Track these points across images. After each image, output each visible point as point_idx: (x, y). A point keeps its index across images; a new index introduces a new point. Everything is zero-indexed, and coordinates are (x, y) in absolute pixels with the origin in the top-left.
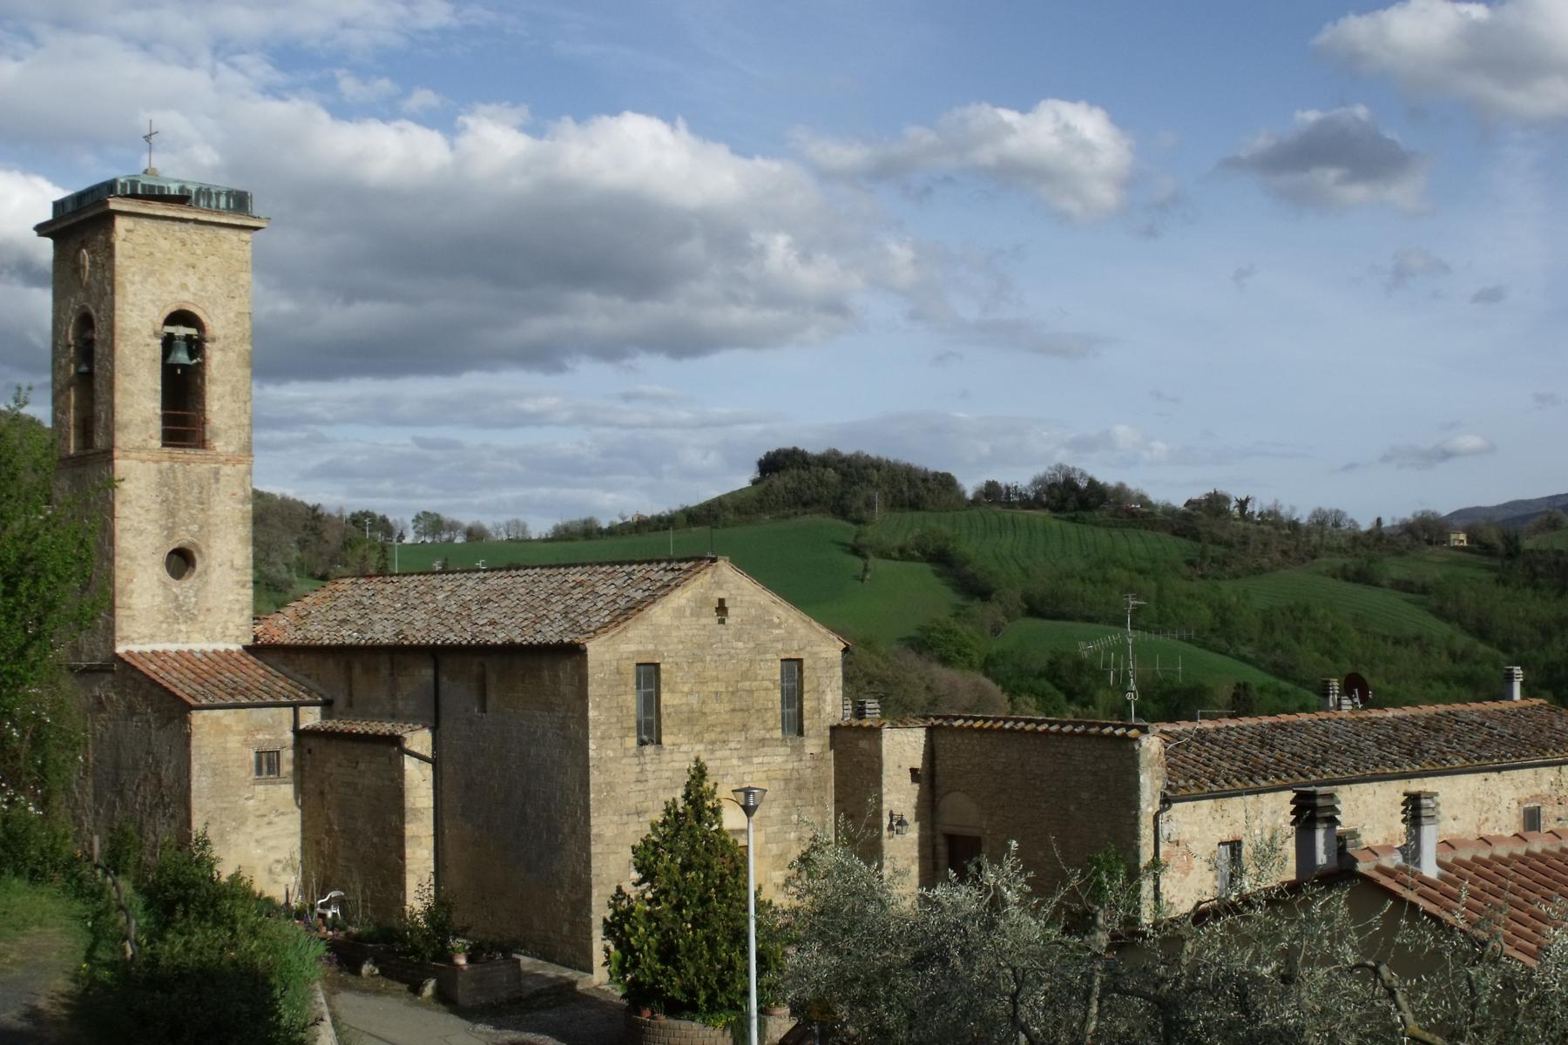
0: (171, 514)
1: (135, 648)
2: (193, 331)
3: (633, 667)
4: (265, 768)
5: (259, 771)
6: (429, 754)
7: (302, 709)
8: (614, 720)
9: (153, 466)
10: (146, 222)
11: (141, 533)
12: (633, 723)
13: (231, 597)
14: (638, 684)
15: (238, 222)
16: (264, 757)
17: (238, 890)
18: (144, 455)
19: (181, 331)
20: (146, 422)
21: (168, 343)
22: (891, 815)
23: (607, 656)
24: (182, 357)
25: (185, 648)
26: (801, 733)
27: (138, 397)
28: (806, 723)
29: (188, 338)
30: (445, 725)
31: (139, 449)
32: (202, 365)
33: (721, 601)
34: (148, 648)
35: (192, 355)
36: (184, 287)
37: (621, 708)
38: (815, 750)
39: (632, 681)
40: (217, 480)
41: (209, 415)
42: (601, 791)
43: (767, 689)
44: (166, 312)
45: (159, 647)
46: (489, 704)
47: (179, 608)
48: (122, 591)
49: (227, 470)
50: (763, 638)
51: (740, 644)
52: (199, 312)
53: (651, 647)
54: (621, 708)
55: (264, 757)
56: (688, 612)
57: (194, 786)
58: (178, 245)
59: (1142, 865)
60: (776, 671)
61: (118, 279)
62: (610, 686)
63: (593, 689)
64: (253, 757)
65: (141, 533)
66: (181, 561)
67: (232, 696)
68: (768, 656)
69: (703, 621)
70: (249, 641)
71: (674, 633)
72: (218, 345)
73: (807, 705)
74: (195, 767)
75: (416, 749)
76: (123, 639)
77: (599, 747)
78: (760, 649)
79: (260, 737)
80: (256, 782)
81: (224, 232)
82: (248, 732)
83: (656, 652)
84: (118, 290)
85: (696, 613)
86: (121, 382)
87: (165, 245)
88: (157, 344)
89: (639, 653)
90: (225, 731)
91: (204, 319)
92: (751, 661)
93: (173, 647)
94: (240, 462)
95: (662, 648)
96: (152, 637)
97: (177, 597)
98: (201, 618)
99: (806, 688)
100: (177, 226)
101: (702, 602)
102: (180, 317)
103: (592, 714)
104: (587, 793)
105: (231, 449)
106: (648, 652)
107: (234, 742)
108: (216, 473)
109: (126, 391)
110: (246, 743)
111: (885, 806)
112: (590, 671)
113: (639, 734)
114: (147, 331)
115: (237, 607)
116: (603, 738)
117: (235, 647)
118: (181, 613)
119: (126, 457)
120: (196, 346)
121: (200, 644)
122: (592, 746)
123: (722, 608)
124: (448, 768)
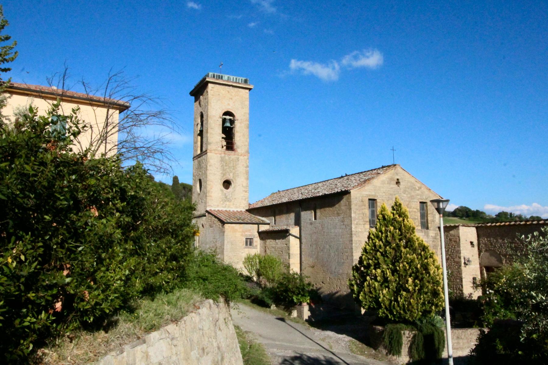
0: (224, 170)
1: (213, 209)
2: (231, 118)
3: (367, 200)
4: (249, 243)
5: (246, 244)
6: (292, 215)
7: (260, 225)
8: (361, 218)
9: (220, 155)
10: (218, 86)
11: (215, 175)
12: (368, 220)
13: (242, 195)
14: (369, 208)
15: (245, 86)
16: (249, 240)
17: (228, 269)
18: (216, 152)
19: (228, 117)
20: (217, 143)
21: (224, 121)
22: (464, 258)
23: (358, 195)
24: (228, 124)
25: (228, 210)
26: (427, 228)
27: (215, 135)
28: (429, 225)
29: (230, 119)
30: (303, 223)
31: (215, 150)
32: (233, 128)
33: (398, 179)
34: (217, 209)
35: (231, 125)
36: (229, 104)
37: (363, 214)
38: (433, 235)
39: (367, 205)
40: (238, 161)
41: (236, 142)
42: (356, 243)
43: (415, 212)
44: (223, 112)
45: (220, 209)
46: (317, 217)
47: (226, 197)
48: (209, 191)
49: (241, 158)
50: (413, 194)
51: (405, 195)
52: (233, 112)
53: (373, 193)
54: (363, 214)
55: (249, 240)
56: (386, 182)
57: (225, 248)
58: (227, 92)
59: (515, 319)
60: (418, 206)
61: (209, 101)
62: (359, 206)
63: (353, 206)
64: (245, 240)
65: (215, 175)
66: (227, 184)
67: (238, 220)
68: (415, 200)
69: (392, 186)
70: (247, 208)
71: (382, 189)
72: (239, 121)
73: (429, 219)
74: (226, 242)
75: (294, 234)
76: (209, 206)
77: (356, 227)
78: (412, 197)
79: (247, 233)
80: (245, 248)
81: (240, 90)
82: (243, 231)
83: (375, 196)
84: (209, 104)
85: (389, 183)
86: (210, 131)
87: (223, 92)
88: (221, 120)
89: (370, 195)
90: (235, 231)
91: (235, 114)
92: (409, 202)
93: (224, 209)
94: (245, 156)
95: (377, 194)
96: (218, 206)
97: (225, 194)
98: (233, 201)
99: (429, 212)
100: (227, 87)
101: (391, 179)
102: (227, 113)
103: (353, 215)
104: (352, 244)
105: (243, 152)
106: (373, 195)
107: (238, 234)
108: (238, 158)
109: (211, 133)
110: (242, 235)
111: (462, 255)
112: (352, 200)
113: (370, 224)
114: (218, 116)
115: (244, 198)
116: (357, 224)
117: (244, 210)
118: (226, 199)
119: (211, 152)
120: (232, 122)
121: (233, 209)
122: (353, 226)
123: (398, 183)
124: (303, 240)
